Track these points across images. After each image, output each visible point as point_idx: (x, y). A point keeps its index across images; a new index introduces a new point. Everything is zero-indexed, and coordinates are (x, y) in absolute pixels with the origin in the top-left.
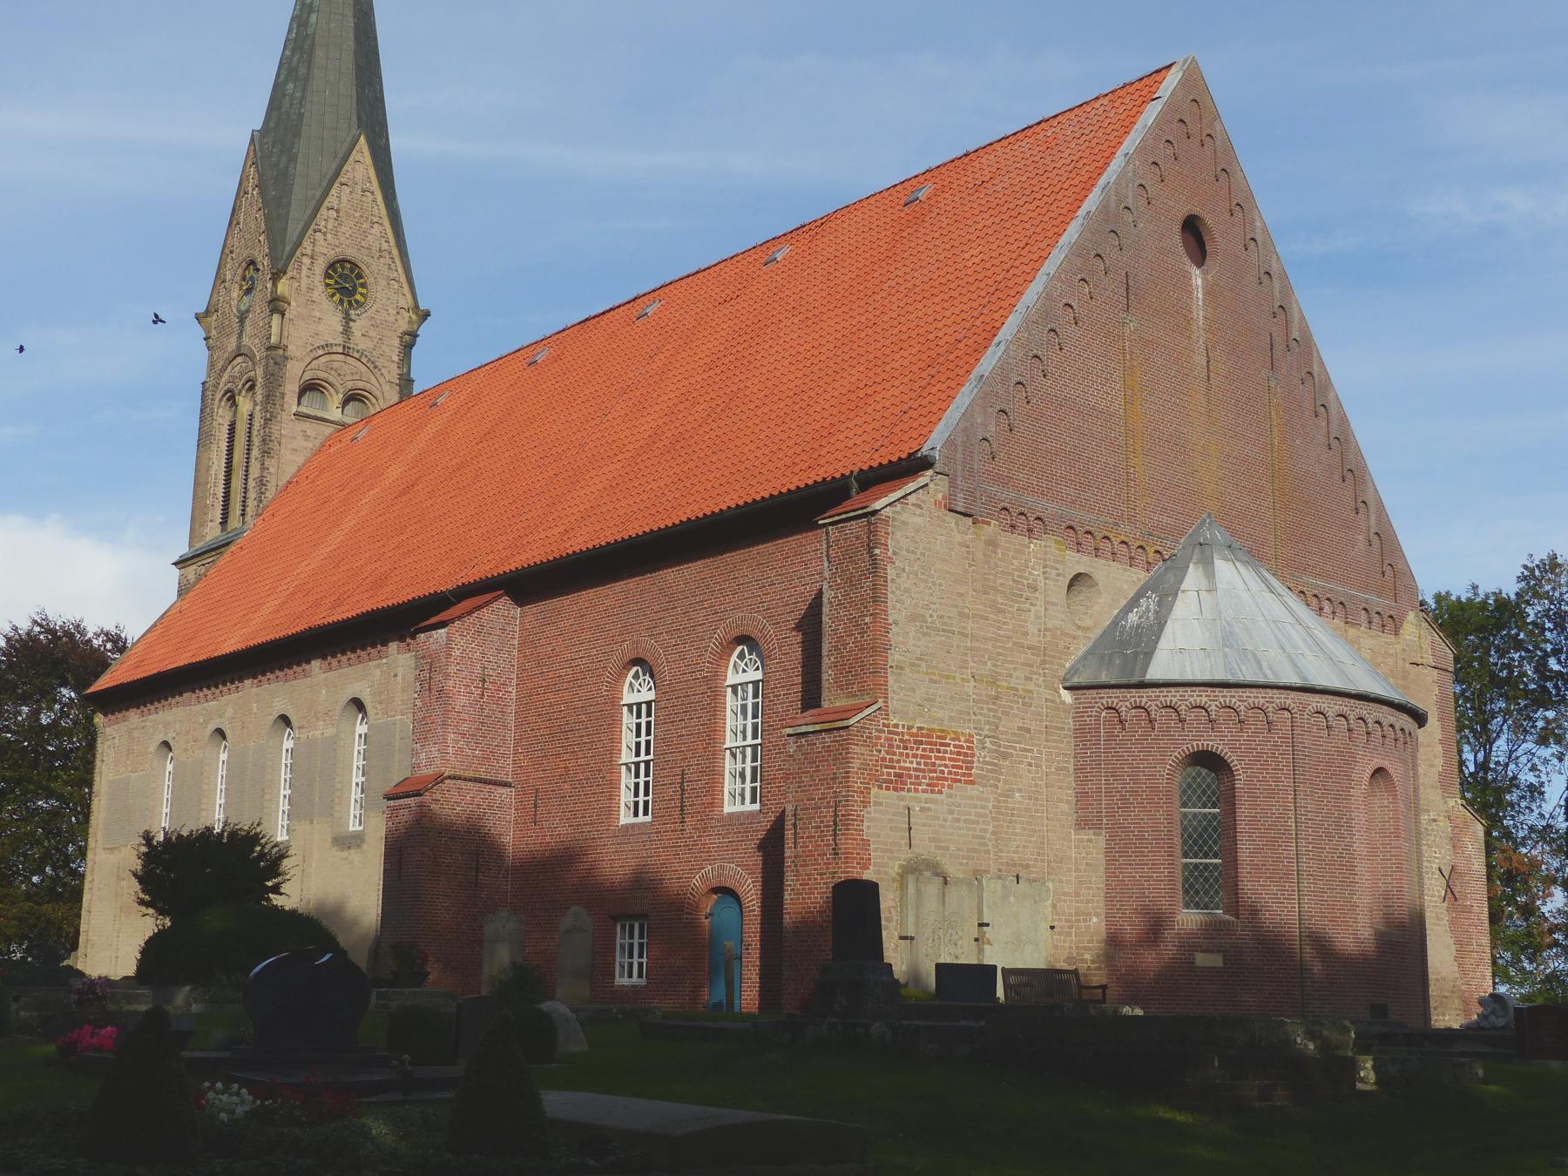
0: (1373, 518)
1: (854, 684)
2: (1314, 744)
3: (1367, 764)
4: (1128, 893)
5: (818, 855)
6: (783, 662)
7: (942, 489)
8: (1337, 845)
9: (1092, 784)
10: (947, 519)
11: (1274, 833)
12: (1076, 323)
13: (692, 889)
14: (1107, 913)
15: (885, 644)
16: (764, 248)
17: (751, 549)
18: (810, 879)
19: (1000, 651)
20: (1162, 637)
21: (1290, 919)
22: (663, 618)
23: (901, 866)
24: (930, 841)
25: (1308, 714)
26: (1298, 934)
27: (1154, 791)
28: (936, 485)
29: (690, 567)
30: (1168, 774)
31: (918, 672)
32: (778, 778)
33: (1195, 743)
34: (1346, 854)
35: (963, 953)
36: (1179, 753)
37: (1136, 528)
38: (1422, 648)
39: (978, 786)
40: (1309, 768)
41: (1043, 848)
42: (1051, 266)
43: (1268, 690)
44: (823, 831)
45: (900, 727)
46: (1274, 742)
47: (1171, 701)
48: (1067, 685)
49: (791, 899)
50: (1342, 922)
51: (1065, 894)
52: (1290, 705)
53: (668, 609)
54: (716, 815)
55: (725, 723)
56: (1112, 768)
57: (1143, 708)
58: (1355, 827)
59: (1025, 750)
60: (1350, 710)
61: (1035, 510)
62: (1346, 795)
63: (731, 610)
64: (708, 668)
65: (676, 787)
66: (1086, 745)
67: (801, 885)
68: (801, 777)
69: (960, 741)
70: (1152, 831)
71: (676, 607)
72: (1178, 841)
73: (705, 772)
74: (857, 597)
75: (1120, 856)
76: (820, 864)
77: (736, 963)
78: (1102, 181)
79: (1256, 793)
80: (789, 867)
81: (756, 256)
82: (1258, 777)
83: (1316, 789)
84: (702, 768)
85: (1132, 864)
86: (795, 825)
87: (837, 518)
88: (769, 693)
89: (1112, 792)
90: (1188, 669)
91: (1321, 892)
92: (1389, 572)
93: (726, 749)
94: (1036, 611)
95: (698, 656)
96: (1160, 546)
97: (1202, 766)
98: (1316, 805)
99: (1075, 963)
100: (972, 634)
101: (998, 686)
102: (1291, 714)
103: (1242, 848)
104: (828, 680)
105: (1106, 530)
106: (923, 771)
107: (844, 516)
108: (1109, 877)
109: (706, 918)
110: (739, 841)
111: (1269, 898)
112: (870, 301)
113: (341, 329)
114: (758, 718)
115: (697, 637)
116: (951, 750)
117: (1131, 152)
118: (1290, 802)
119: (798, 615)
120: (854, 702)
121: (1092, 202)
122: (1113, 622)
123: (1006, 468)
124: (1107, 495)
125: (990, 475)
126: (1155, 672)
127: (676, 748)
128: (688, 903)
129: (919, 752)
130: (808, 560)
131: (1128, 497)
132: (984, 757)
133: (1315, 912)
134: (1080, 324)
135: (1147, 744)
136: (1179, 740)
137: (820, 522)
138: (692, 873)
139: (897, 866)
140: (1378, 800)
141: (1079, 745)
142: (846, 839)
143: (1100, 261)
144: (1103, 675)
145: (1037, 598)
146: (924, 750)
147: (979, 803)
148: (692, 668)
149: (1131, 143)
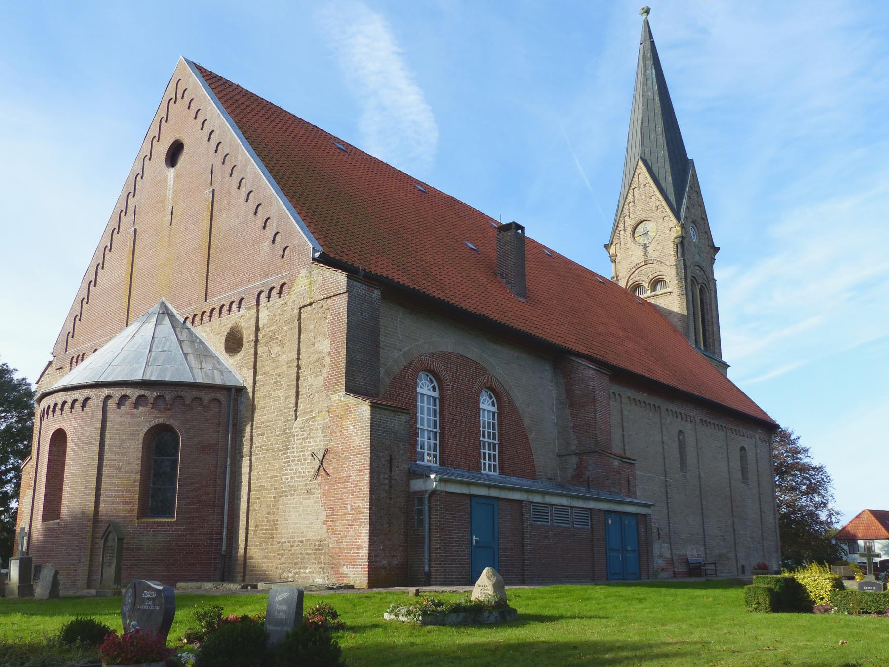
113: (642, 254)
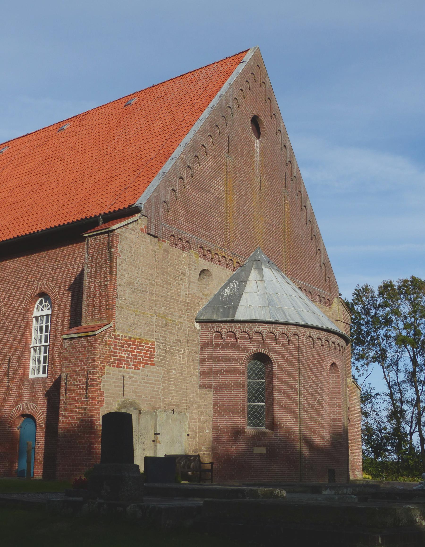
0: (322, 257)
1: (98, 314)
2: (308, 351)
3: (329, 361)
4: (224, 419)
5: (78, 399)
6: (62, 306)
7: (145, 223)
8: (316, 397)
9: (208, 367)
10: (146, 238)
11: (290, 392)
12: (206, 155)
13: (12, 415)
14: (213, 428)
15: (114, 295)
16: (58, 125)
17: (48, 252)
18: (73, 411)
19: (168, 302)
20: (241, 300)
21: (296, 431)
22: (3, 284)
23: (119, 405)
24: (133, 393)
25: (305, 337)
26: (299, 438)
27: (237, 371)
28: (142, 221)
29: (17, 260)
30: (243, 363)
31: (130, 310)
32: (57, 362)
33: (256, 349)
34: (320, 401)
35: (147, 448)
36: (249, 354)
37: (229, 250)
38: (339, 313)
39: (156, 367)
40: (306, 362)
41: (185, 397)
42: (198, 125)
43: (289, 326)
44: (81, 387)
45: (121, 337)
46: (291, 349)
47: (246, 329)
48: (198, 320)
49: (63, 421)
50: (317, 432)
51: (194, 419)
52: (298, 333)
53: (5, 280)
54: (25, 379)
55: (31, 335)
56: (217, 360)
57: (233, 332)
58: (323, 389)
59: (178, 350)
60: (323, 336)
61: (186, 238)
62: (320, 375)
63: (37, 280)
64: (24, 308)
65: (6, 365)
66: (206, 349)
67: (68, 413)
68: (70, 360)
69: (148, 344)
70: (235, 390)
71: (10, 279)
72: (246, 394)
73: (21, 358)
74: (102, 272)
75: (220, 401)
76: (78, 403)
77: (33, 451)
78: (219, 94)
79: (283, 373)
80: (62, 404)
81: (54, 128)
82: (284, 365)
83: (308, 371)
84: (19, 356)
85: (225, 405)
86: (66, 384)
87: (93, 233)
88: (54, 320)
89: (217, 371)
90: (253, 314)
91: (309, 419)
92: (328, 281)
93: (31, 347)
94: (185, 285)
95: (20, 302)
96: (239, 260)
97: (259, 360)
98: (308, 379)
99: (197, 452)
100: (156, 293)
101: (167, 319)
102: (299, 337)
103: (276, 398)
104: (85, 312)
105: (217, 250)
106: (131, 358)
107: (96, 233)
108: (215, 411)
109: (18, 429)
110: (36, 392)
111: (287, 421)
112: (109, 144)
114: (48, 332)
115: (20, 293)
116: (144, 349)
117: (232, 83)
118: (297, 377)
119: (70, 283)
120: (98, 323)
121: (215, 102)
122: (218, 293)
123: (173, 217)
124: (217, 234)
125: (166, 219)
126: (238, 316)
127: (7, 347)
128: (9, 422)
129: (129, 349)
130: (76, 257)
131: (226, 236)
132: (160, 353)
133: (307, 428)
134: (208, 155)
135: (234, 349)
136: (248, 347)
137: (84, 235)
138: (12, 407)
139: (117, 405)
140: (331, 377)
141: (202, 349)
142: (93, 391)
143: (217, 129)
144: (215, 316)
145: (185, 279)
146: (132, 348)
147: (157, 375)
148: (16, 308)
149: (232, 79)
